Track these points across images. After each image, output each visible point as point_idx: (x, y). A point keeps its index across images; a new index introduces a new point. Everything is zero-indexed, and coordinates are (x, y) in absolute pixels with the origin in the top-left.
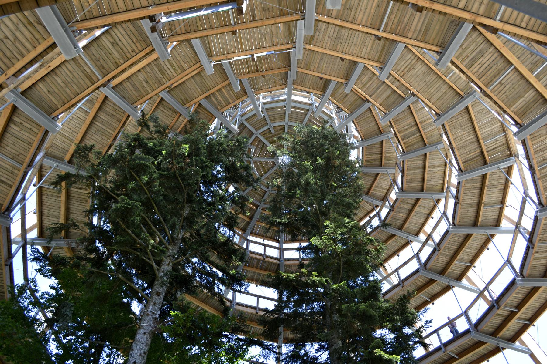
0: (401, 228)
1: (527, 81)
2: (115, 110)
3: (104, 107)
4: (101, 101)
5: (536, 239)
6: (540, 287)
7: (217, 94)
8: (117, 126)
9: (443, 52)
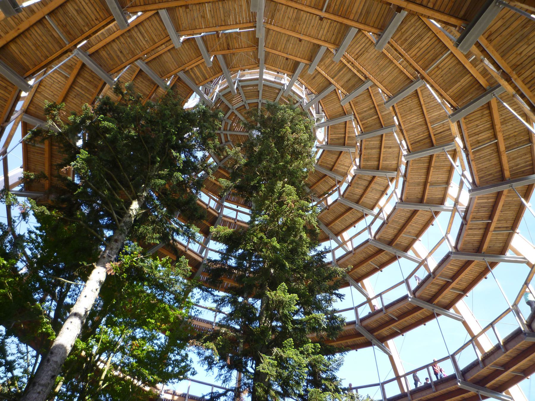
0: (357, 202)
1: (464, 66)
2: (93, 77)
3: (83, 74)
4: (79, 68)
5: (469, 217)
6: (473, 261)
7: (195, 69)
8: (94, 92)
9: (381, 34)
